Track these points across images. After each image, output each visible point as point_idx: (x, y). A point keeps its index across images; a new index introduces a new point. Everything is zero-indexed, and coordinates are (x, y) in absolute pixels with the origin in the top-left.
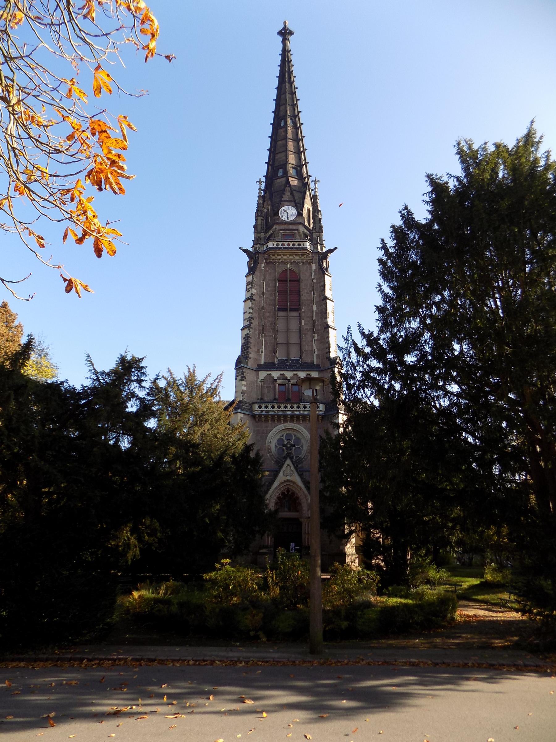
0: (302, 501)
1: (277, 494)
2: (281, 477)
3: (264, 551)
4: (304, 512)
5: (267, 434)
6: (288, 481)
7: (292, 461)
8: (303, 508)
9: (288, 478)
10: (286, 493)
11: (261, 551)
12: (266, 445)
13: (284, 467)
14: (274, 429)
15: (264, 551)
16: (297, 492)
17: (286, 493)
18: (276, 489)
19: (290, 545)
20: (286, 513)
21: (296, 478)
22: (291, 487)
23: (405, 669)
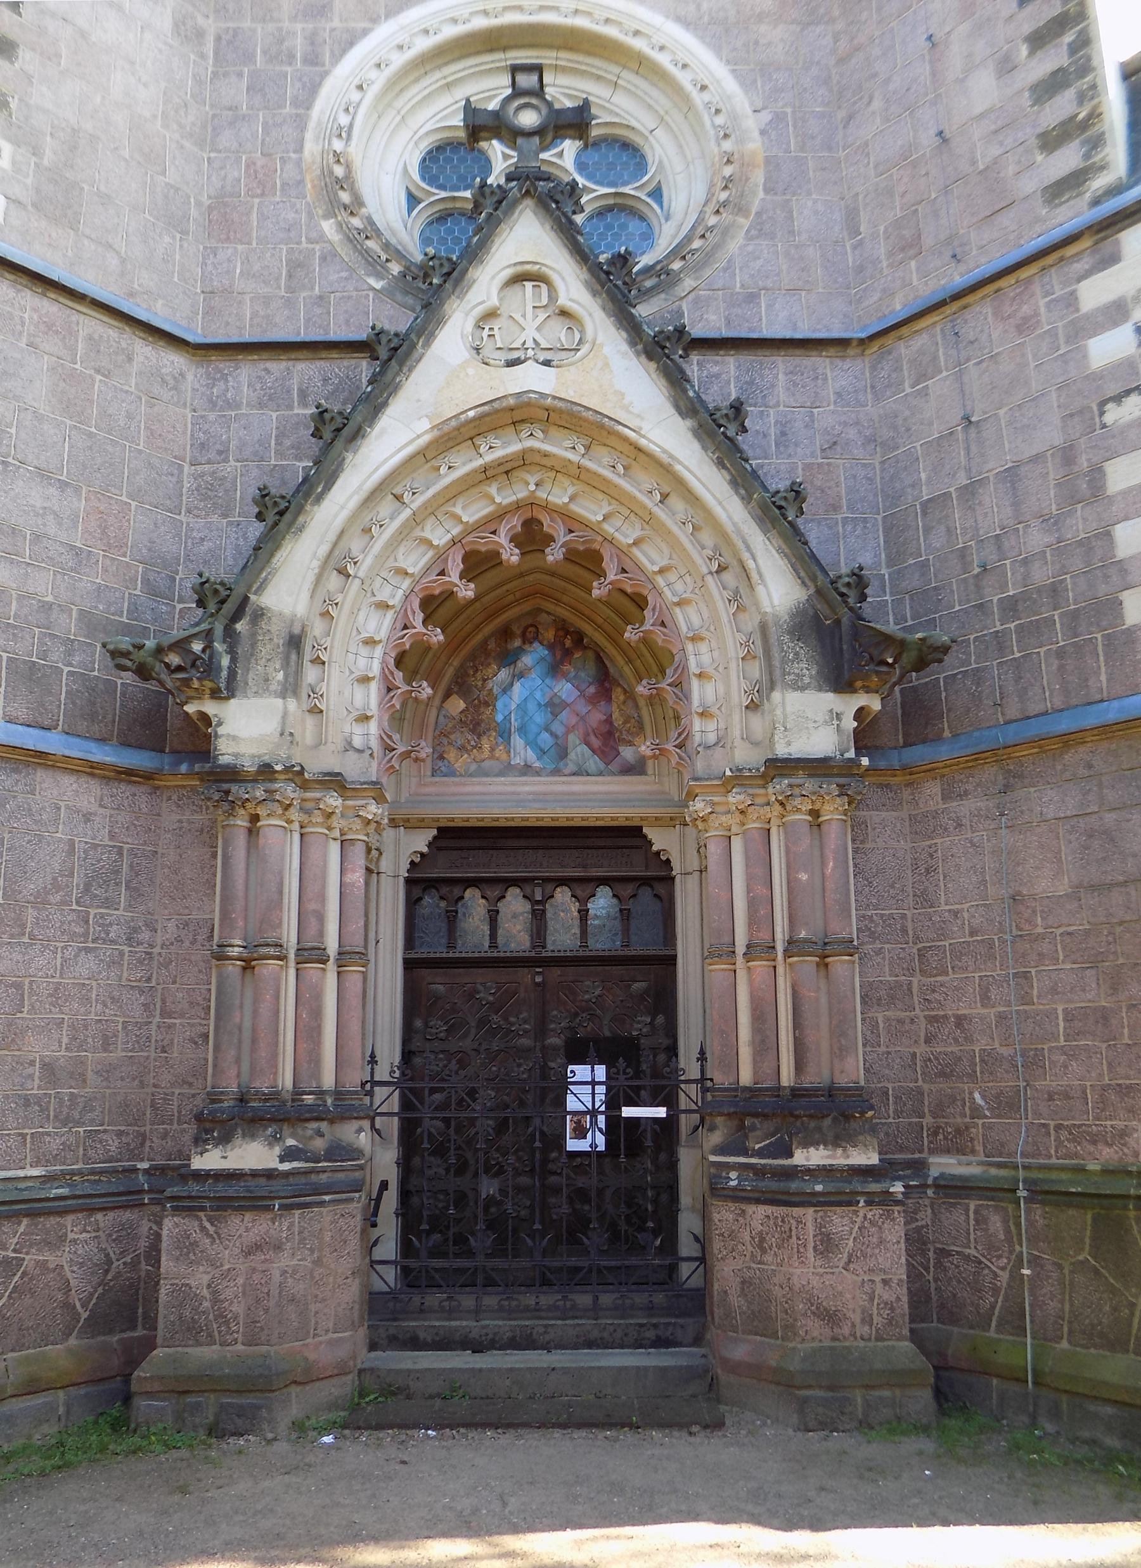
0: (686, 619)
1: (415, 561)
2: (448, 376)
3: (252, 1154)
4: (701, 730)
5: (317, 63)
6: (517, 414)
7: (568, 232)
8: (700, 693)
9: (532, 379)
10: (511, 555)
11: (210, 1160)
12: (311, 148)
13: (485, 283)
14: (384, 33)
15: (252, 1154)
16: (624, 533)
17: (511, 555)
18: (387, 488)
19: (563, 1086)
20: (529, 786)
21: (620, 384)
22: (558, 495)
23: (1033, 1358)
